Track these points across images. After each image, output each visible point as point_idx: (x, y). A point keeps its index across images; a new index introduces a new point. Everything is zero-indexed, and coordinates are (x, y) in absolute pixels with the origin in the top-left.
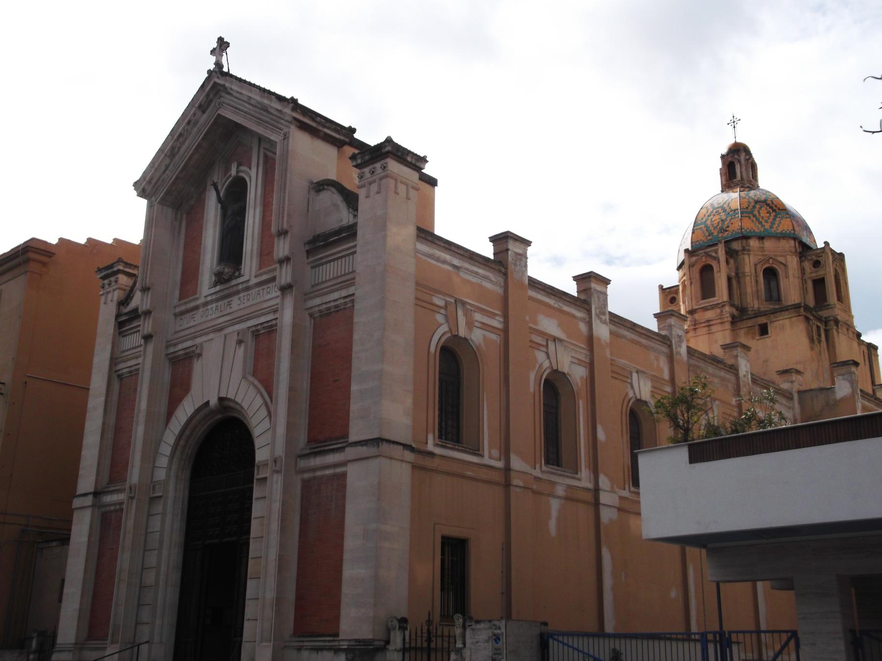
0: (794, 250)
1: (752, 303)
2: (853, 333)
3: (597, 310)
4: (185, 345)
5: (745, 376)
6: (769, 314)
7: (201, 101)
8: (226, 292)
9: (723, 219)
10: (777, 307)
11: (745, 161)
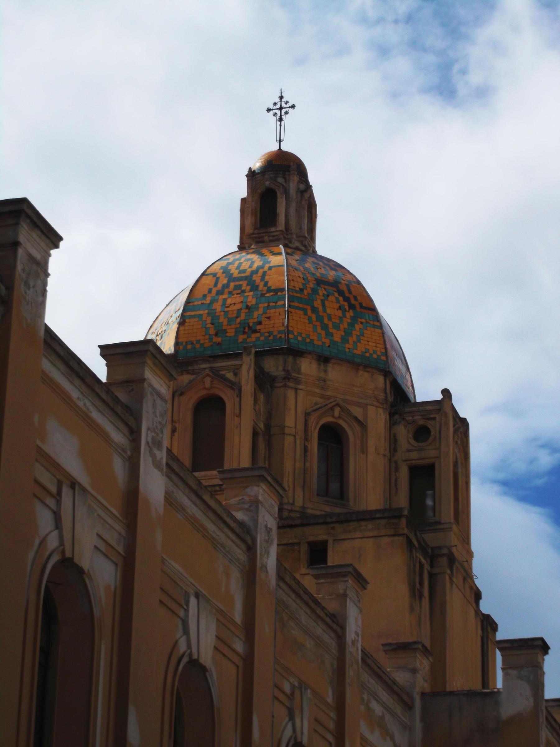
0: (382, 396)
1: (290, 494)
2: (471, 588)
3: (150, 435)
5: (353, 642)
6: (332, 523)
9: (250, 304)
10: (338, 510)
11: (297, 194)
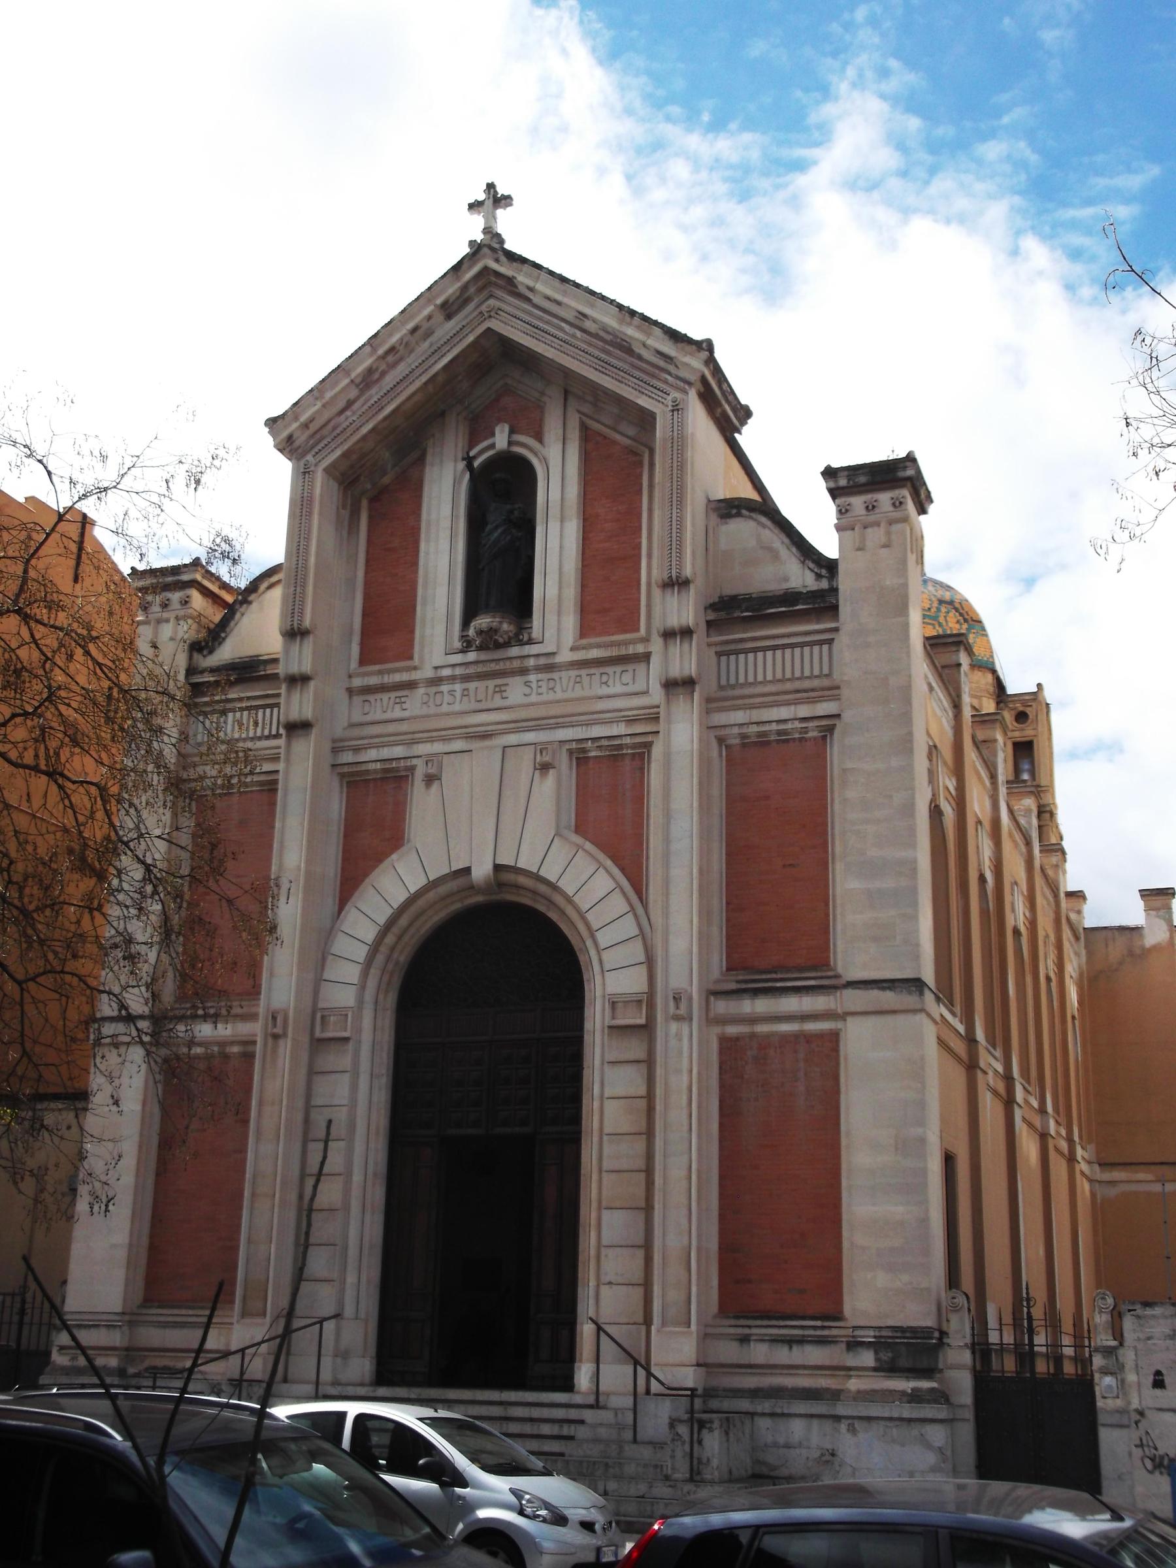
4: (386, 753)
7: (450, 296)
8: (493, 667)
